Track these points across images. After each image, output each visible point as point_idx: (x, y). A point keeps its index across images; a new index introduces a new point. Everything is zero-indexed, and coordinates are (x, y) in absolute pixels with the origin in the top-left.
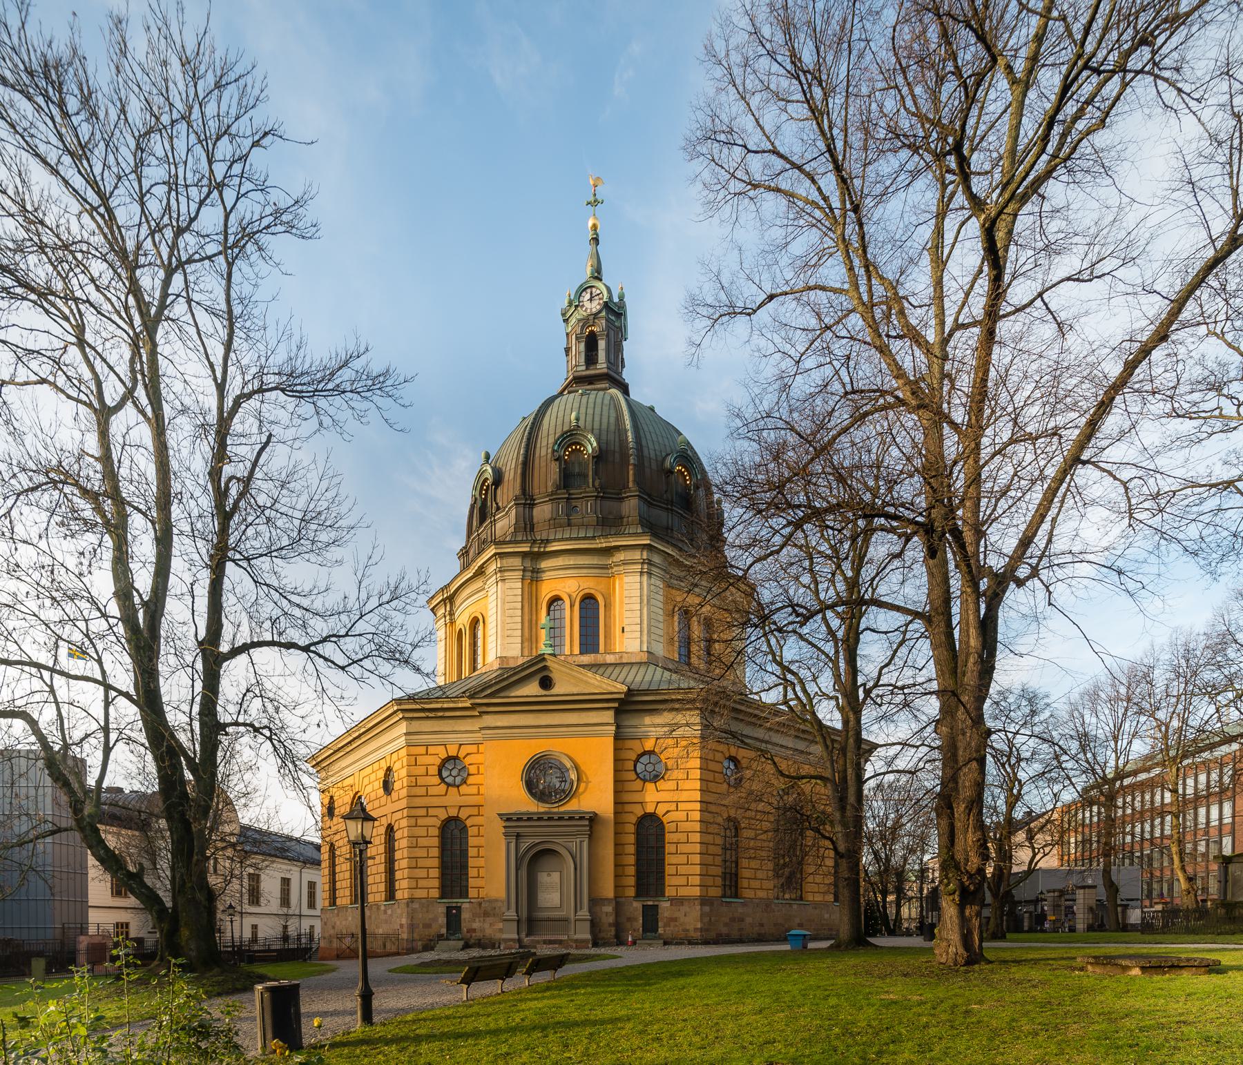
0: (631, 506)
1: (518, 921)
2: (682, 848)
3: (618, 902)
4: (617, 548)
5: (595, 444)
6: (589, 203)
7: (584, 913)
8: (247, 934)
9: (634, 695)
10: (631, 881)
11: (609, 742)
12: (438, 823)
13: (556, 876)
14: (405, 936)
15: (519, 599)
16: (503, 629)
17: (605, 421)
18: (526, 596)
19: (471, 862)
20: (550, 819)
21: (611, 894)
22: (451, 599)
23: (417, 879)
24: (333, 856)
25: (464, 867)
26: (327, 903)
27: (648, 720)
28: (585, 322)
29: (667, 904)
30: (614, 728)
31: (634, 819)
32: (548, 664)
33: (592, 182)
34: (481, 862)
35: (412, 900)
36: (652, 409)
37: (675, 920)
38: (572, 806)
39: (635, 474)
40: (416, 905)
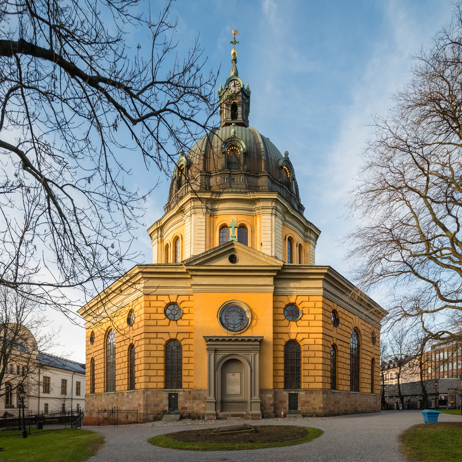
0: (263, 181)
1: (216, 403)
2: (311, 360)
3: (275, 391)
4: (259, 200)
5: (244, 146)
6: (231, 42)
7: (257, 398)
8: (42, 409)
9: (286, 269)
10: (282, 379)
11: (270, 296)
12: (164, 342)
13: (238, 376)
14: (142, 411)
15: (204, 224)
16: (195, 240)
17: (248, 138)
18: (208, 223)
19: (184, 367)
20: (236, 340)
21: (271, 387)
22: (161, 228)
23: (150, 376)
24: (93, 370)
25: (180, 370)
26: (89, 392)
27: (292, 284)
28: (231, 97)
29: (303, 393)
30: (273, 288)
31: (283, 343)
32: (235, 247)
33: (233, 32)
34: (191, 367)
35: (147, 389)
36: (269, 139)
37: (308, 402)
38: (248, 333)
39: (265, 165)
40: (149, 393)
